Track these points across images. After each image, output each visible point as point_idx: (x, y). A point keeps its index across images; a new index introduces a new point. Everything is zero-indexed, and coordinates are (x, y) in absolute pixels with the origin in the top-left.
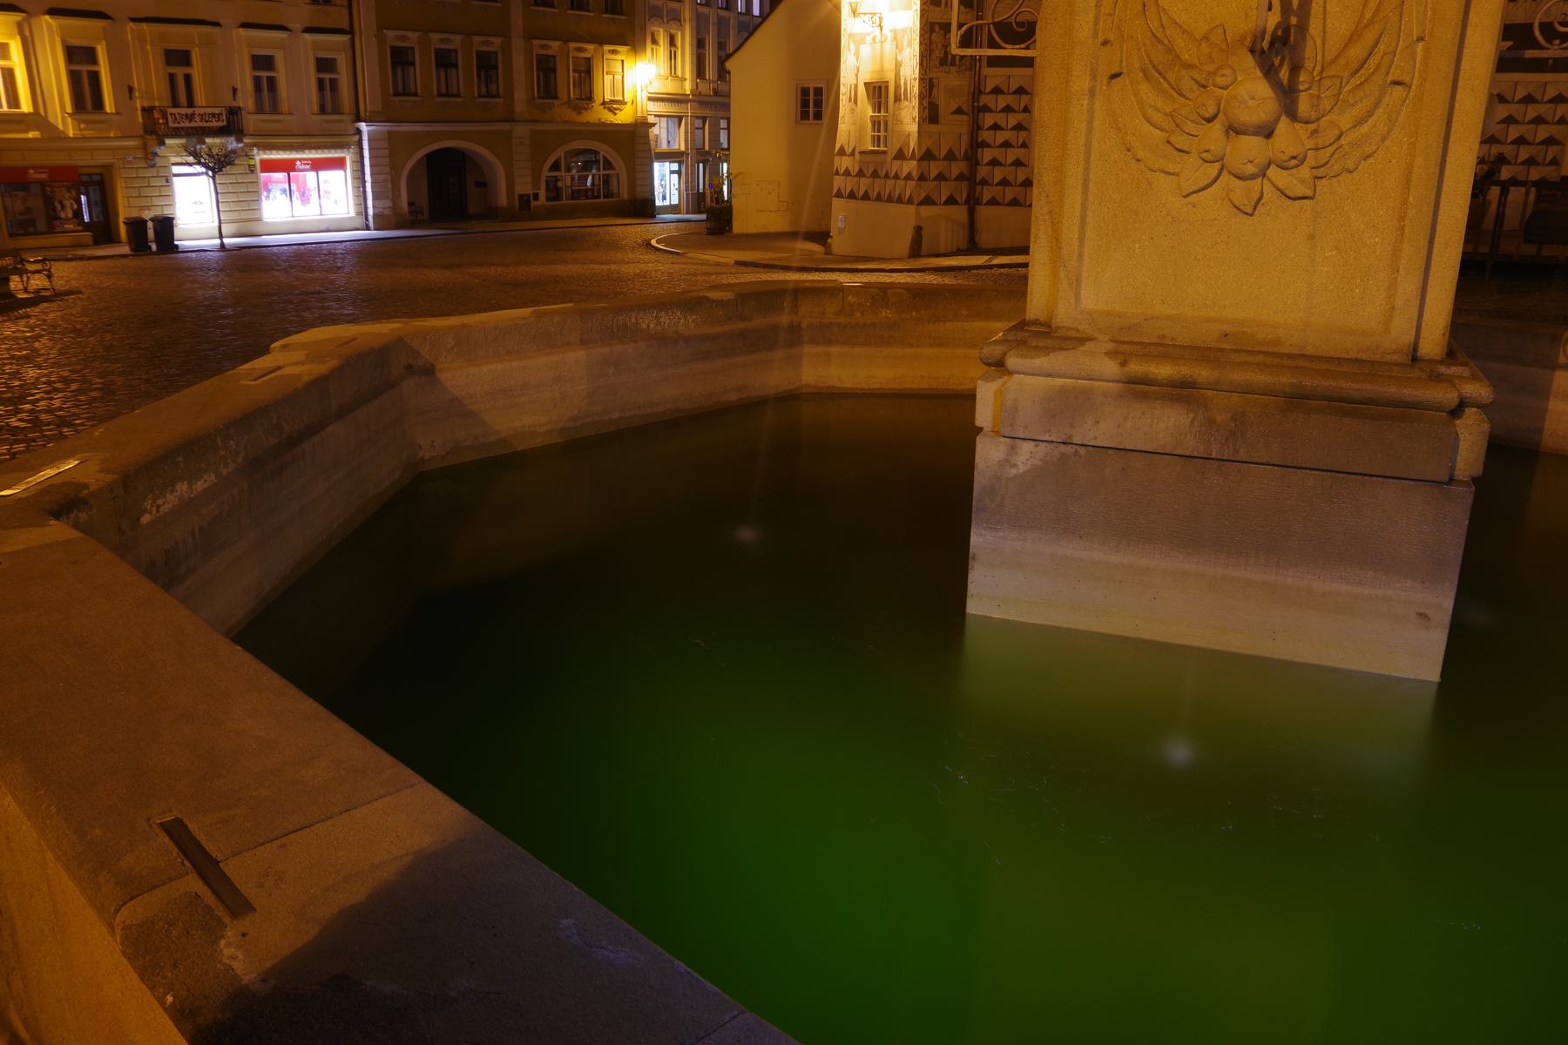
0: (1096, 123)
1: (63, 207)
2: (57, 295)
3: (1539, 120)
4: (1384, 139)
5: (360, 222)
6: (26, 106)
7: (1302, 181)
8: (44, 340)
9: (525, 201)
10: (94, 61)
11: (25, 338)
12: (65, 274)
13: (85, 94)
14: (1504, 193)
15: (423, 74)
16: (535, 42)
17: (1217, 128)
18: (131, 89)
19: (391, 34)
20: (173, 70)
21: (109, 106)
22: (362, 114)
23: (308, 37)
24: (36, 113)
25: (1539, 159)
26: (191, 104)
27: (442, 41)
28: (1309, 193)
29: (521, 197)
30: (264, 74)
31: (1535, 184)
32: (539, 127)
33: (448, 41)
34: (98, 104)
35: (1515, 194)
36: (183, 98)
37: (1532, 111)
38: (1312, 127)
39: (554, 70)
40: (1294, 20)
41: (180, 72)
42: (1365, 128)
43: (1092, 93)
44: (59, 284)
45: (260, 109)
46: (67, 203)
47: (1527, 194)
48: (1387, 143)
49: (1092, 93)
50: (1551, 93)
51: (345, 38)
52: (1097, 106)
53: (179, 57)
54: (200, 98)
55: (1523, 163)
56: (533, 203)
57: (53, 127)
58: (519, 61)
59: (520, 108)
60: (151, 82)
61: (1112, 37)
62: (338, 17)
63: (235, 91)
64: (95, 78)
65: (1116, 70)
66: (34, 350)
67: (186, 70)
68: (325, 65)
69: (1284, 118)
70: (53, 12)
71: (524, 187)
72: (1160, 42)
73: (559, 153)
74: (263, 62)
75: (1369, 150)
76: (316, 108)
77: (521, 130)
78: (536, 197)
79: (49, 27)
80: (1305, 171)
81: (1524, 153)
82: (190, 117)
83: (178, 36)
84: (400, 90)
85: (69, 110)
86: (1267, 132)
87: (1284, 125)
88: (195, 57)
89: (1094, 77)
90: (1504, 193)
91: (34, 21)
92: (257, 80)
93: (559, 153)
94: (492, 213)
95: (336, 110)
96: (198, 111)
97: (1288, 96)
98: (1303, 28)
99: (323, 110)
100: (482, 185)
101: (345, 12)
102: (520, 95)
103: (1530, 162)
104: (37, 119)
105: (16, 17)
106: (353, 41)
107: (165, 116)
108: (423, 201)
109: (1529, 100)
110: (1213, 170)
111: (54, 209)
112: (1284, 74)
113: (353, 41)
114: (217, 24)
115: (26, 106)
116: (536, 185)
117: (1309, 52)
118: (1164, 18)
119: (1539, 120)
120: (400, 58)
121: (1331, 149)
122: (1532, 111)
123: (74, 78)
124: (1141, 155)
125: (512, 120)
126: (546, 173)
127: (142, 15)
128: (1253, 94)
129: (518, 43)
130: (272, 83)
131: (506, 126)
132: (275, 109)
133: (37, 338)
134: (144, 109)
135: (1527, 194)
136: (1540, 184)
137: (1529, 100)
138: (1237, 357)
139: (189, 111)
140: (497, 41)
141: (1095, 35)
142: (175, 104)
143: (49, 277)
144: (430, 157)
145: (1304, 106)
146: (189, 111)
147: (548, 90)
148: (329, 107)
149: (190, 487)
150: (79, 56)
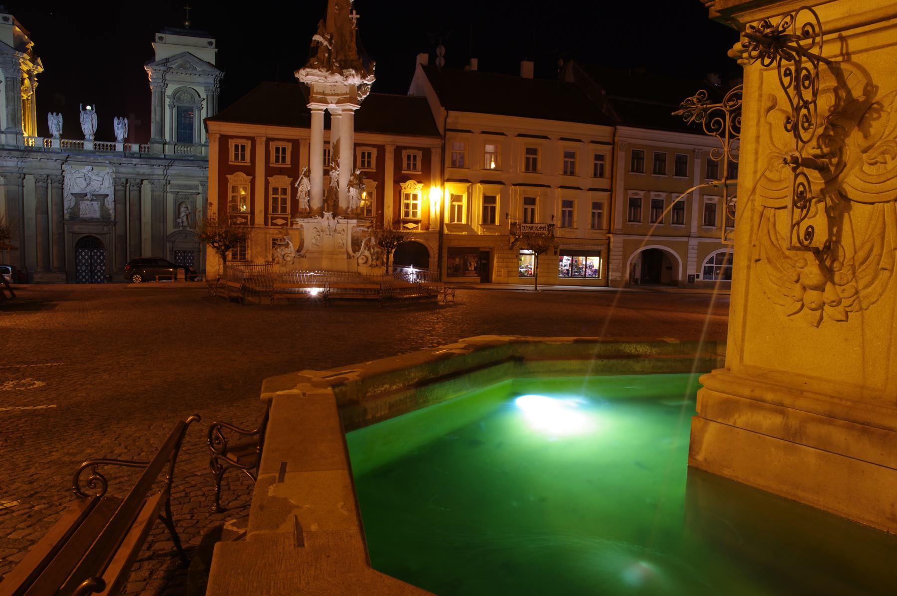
0: (751, 280)
2: (455, 304)
4: (881, 295)
5: (603, 282)
6: (464, 221)
9: (691, 278)
10: (495, 202)
12: (461, 295)
15: (645, 211)
17: (798, 287)
18: (507, 215)
19: (630, 192)
20: (526, 206)
21: (497, 222)
23: (590, 193)
24: (467, 224)
26: (532, 222)
28: (844, 318)
29: (689, 276)
32: (703, 240)
33: (659, 196)
34: (493, 221)
36: (529, 219)
38: (842, 288)
39: (714, 211)
40: (834, 239)
41: (529, 207)
42: (870, 289)
43: (749, 267)
44: (458, 299)
45: (563, 226)
48: (883, 297)
49: (749, 267)
52: (752, 273)
53: (530, 201)
56: (696, 280)
58: (695, 206)
59: (694, 229)
60: (516, 212)
61: (757, 243)
63: (553, 217)
64: (494, 209)
65: (757, 258)
66: (434, 329)
67: (532, 207)
68: (597, 206)
70: (482, 182)
71: (691, 271)
72: (775, 246)
74: (568, 204)
75: (873, 300)
76: (589, 227)
77: (693, 242)
78: (698, 276)
80: (841, 308)
82: (531, 228)
83: (531, 192)
86: (821, 288)
87: (829, 286)
88: (538, 201)
89: (750, 260)
91: (474, 186)
92: (564, 212)
94: (675, 283)
97: (828, 273)
98: (838, 242)
99: (593, 227)
100: (670, 268)
101: (608, 181)
102: (694, 224)
104: (467, 227)
105: (468, 184)
106: (611, 195)
108: (638, 275)
110: (799, 304)
112: (828, 263)
113: (611, 195)
114: (549, 187)
115: (464, 221)
116: (698, 270)
117: (841, 253)
118: (779, 236)
120: (634, 204)
121: (852, 299)
123: (485, 209)
124: (769, 296)
125: (689, 236)
128: (812, 272)
130: (571, 213)
131: (685, 239)
132: (570, 225)
133: (437, 323)
138: (809, 395)
141: (750, 242)
142: (525, 222)
145: (837, 278)
148: (596, 227)
150: (489, 200)
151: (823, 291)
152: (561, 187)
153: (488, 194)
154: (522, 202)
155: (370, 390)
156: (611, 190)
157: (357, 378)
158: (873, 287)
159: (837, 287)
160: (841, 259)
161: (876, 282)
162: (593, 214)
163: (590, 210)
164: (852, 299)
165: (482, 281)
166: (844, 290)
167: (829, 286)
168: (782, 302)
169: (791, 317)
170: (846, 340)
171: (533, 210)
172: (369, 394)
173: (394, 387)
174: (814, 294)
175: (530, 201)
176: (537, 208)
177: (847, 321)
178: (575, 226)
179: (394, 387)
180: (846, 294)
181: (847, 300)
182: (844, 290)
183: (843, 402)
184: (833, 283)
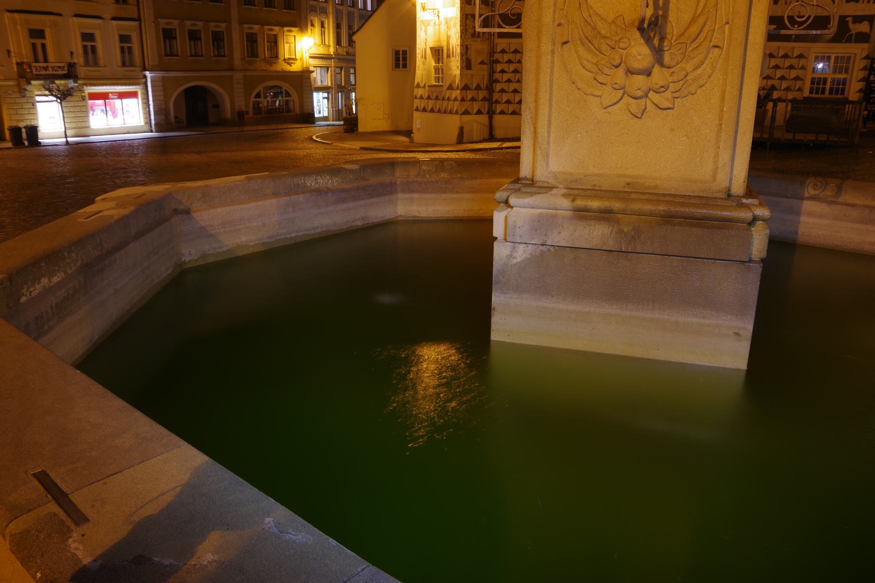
3: (791, 67)
7: (667, 100)
14: (775, 106)
15: (181, 44)
16: (246, 26)
17: (621, 71)
18: (9, 52)
22: (147, 66)
23: (114, 23)
25: (792, 88)
27: (192, 25)
28: (671, 106)
30: (89, 44)
31: (790, 101)
32: (248, 73)
35: (781, 106)
37: (788, 63)
38: (671, 70)
39: (256, 41)
40: (660, 13)
41: (39, 42)
42: (700, 71)
43: (553, 52)
45: (87, 64)
47: (787, 106)
48: (712, 79)
49: (553, 52)
50: (797, 53)
51: (135, 24)
53: (37, 34)
54: (51, 57)
56: (246, 116)
59: (237, 62)
61: (563, 22)
63: (72, 53)
65: (565, 39)
67: (43, 41)
68: (124, 39)
69: (657, 67)
71: (240, 104)
72: (589, 24)
73: (260, 88)
74: (88, 37)
75: (702, 83)
76: (120, 63)
77: (238, 76)
81: (784, 85)
82: (46, 68)
83: (37, 21)
84: (169, 53)
86: (648, 73)
87: (656, 69)
88: (48, 33)
89: (554, 43)
90: (775, 106)
92: (85, 48)
93: (260, 88)
95: (132, 64)
96: (50, 65)
97: (658, 53)
98: (665, 17)
99: (124, 64)
100: (216, 106)
101: (135, 9)
102: (237, 55)
109: (786, 56)
114: (60, 15)
117: (669, 30)
118: (591, 12)
119: (791, 67)
120: (168, 35)
122: (788, 63)
124: (580, 86)
126: (252, 99)
128: (639, 52)
129: (235, 26)
130: (94, 48)
131: (229, 73)
132: (96, 63)
134: (17, 64)
135: (787, 106)
136: (794, 101)
137: (786, 56)
139: (45, 65)
140: (223, 25)
141: (554, 21)
144: (186, 91)
145: (667, 59)
146: (45, 65)
147: (253, 52)
148: (127, 63)
149: (50, 280)
151: (649, 75)
152: (77, 15)
156: (138, 19)
159: (664, 69)
160: (669, 37)
161: (707, 62)
162: (122, 49)
163: (117, 45)
164: (682, 83)
166: (673, 73)
169: (609, 109)
170: (672, 130)
173: (55, 280)
175: (37, 34)
176: (49, 42)
178: (102, 62)
179: (55, 280)
180: (675, 78)
181: (676, 84)
182: (673, 73)
183: (636, 206)
184: (662, 64)
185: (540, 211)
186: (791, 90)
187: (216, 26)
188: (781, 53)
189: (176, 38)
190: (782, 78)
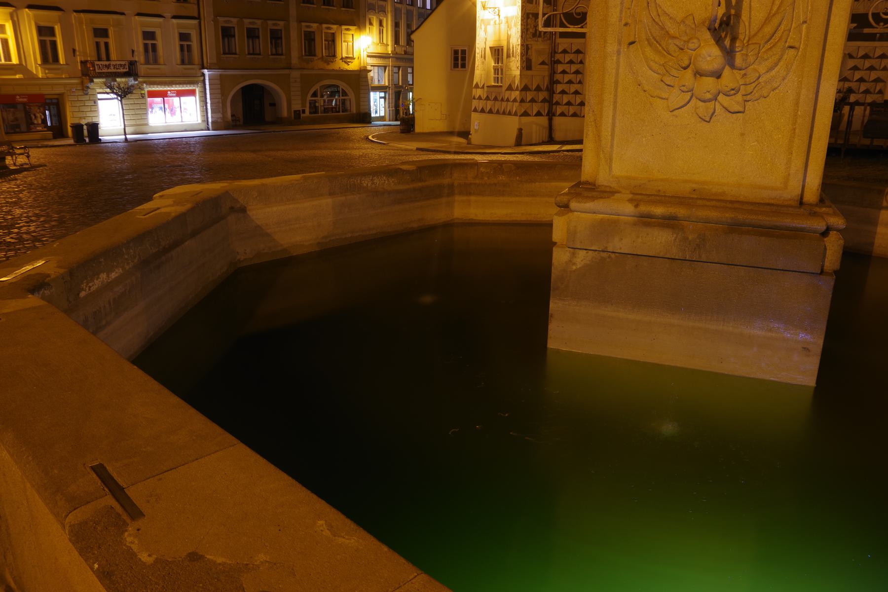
0: (621, 70)
1: (36, 117)
2: (32, 168)
3: (872, 68)
4: (784, 79)
6: (15, 60)
7: (738, 103)
8: (25, 193)
9: (297, 114)
11: (14, 192)
13: (48, 54)
14: (852, 110)
15: (240, 42)
16: (303, 24)
17: (689, 73)
18: (74, 51)
19: (220, 19)
20: (98, 40)
21: (62, 60)
23: (175, 21)
24: (21, 64)
25: (872, 90)
26: (108, 59)
28: (741, 109)
29: (295, 111)
30: (150, 42)
31: (869, 104)
32: (305, 72)
34: (56, 59)
35: (858, 110)
36: (104, 56)
37: (868, 63)
38: (743, 72)
40: (733, 12)
41: (102, 41)
42: (773, 73)
44: (34, 161)
45: (147, 62)
46: (38, 115)
47: (865, 110)
48: (786, 81)
50: (878, 53)
51: (195, 22)
52: (622, 60)
53: (102, 33)
54: (113, 55)
55: (863, 93)
56: (302, 115)
57: (32, 73)
58: (294, 34)
59: (295, 60)
60: (86, 46)
61: (629, 21)
62: (191, 9)
63: (133, 51)
64: (54, 44)
65: (632, 40)
66: (20, 199)
67: (106, 40)
68: (184, 37)
70: (30, 7)
71: (297, 106)
72: (657, 24)
73: (317, 87)
74: (149, 35)
76: (179, 61)
77: (295, 74)
78: (304, 112)
79: (28, 15)
80: (739, 97)
81: (863, 87)
82: (108, 67)
83: (101, 21)
85: (39, 62)
86: (718, 75)
87: (727, 71)
90: (852, 110)
91: (19, 12)
92: (146, 45)
93: (317, 87)
94: (278, 121)
95: (191, 62)
96: (112, 63)
97: (729, 54)
98: (738, 16)
99: (183, 62)
100: (273, 105)
101: (196, 7)
102: (295, 54)
103: (867, 92)
104: (21, 68)
106: (200, 23)
107: (93, 66)
109: (866, 57)
110: (687, 96)
111: (31, 119)
113: (200, 23)
114: (123, 14)
115: (15, 60)
116: (304, 105)
117: (741, 30)
118: (660, 11)
119: (872, 68)
120: (227, 33)
121: (754, 85)
122: (868, 63)
123: (42, 44)
126: (309, 98)
127: (86, 8)
128: (710, 54)
129: (293, 24)
130: (154, 47)
131: (286, 72)
132: (156, 62)
133: (21, 191)
134: (82, 62)
135: (865, 110)
136: (873, 105)
137: (866, 57)
139: (107, 63)
140: (282, 23)
141: (620, 20)
142: (99, 59)
143: (28, 157)
144: (243, 88)
145: (738, 61)
146: (107, 63)
149: (108, 276)
150: (45, 32)
153: (42, 24)
154: (91, 34)
155: (84, 286)
157: (62, 271)
158: (776, 69)
163: (177, 43)
165: (55, 137)
167: (727, 71)
168: (664, 95)
171: (106, 44)
172: (83, 294)
173: (113, 275)
174: (709, 81)
177: (743, 112)
185: (601, 216)
186: (870, 93)
187: (274, 25)
188: (861, 53)
189: (234, 36)
190: (861, 80)
